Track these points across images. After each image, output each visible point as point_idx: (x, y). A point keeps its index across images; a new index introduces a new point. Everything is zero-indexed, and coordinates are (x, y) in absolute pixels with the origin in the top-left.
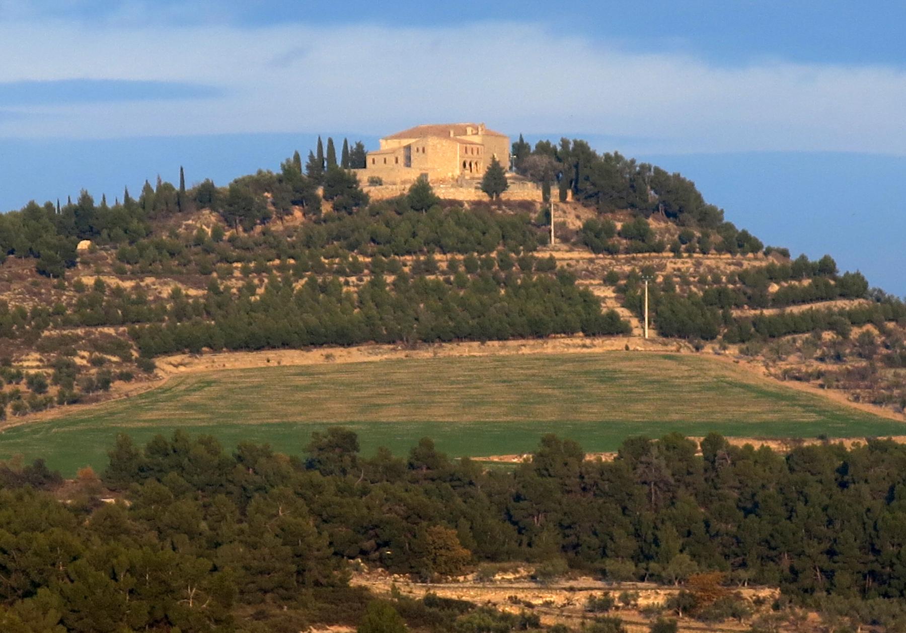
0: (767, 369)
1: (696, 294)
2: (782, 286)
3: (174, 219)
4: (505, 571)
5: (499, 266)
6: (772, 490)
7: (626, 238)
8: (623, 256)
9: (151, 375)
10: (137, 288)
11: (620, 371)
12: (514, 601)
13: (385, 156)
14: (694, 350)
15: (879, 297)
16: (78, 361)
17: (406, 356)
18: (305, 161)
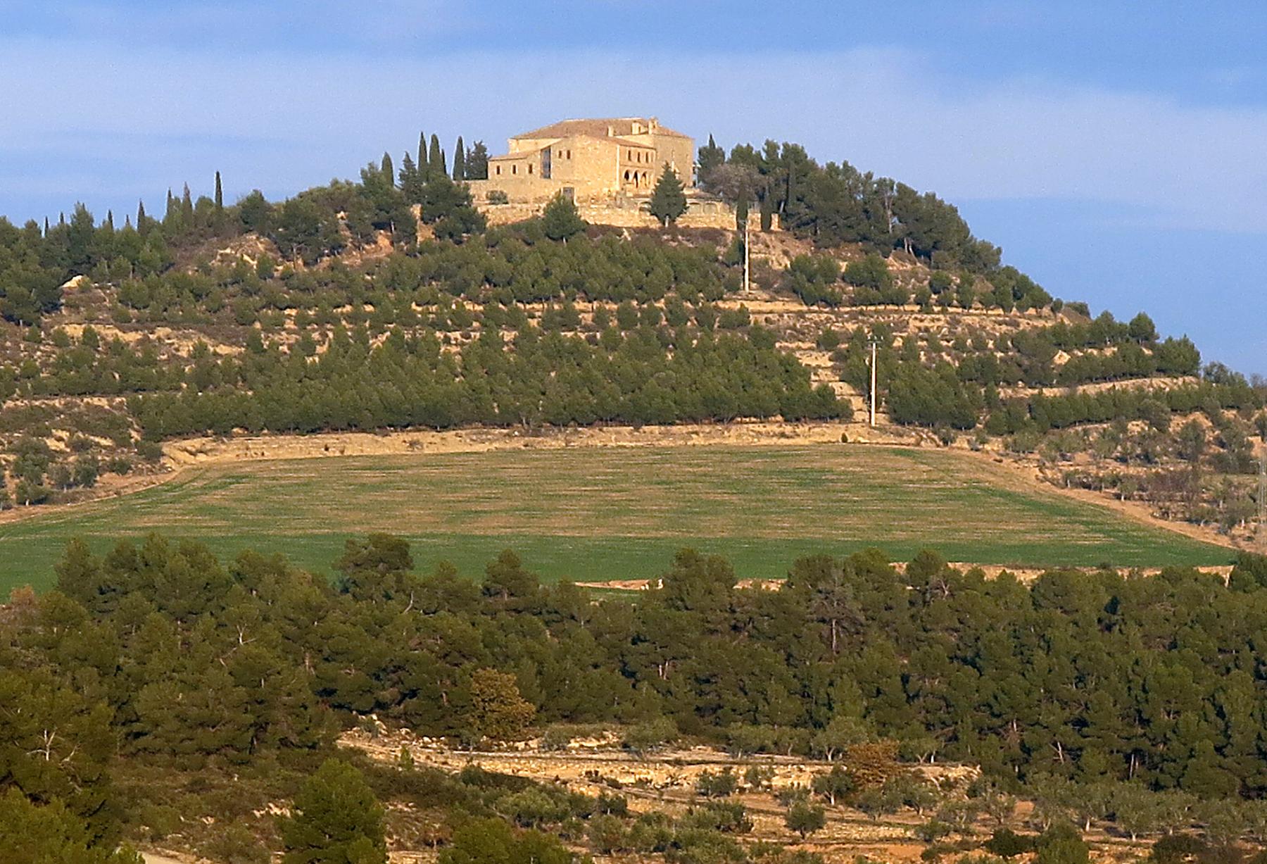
0: (1041, 471)
1: (948, 364)
2: (1073, 356)
3: (206, 246)
4: (585, 736)
5: (667, 320)
6: (1002, 633)
7: (852, 284)
8: (848, 309)
9: (157, 466)
10: (144, 342)
11: (830, 471)
12: (594, 778)
13: (498, 164)
14: (941, 443)
15: (1218, 375)
16: (52, 444)
17: (526, 446)
18: (398, 167)
